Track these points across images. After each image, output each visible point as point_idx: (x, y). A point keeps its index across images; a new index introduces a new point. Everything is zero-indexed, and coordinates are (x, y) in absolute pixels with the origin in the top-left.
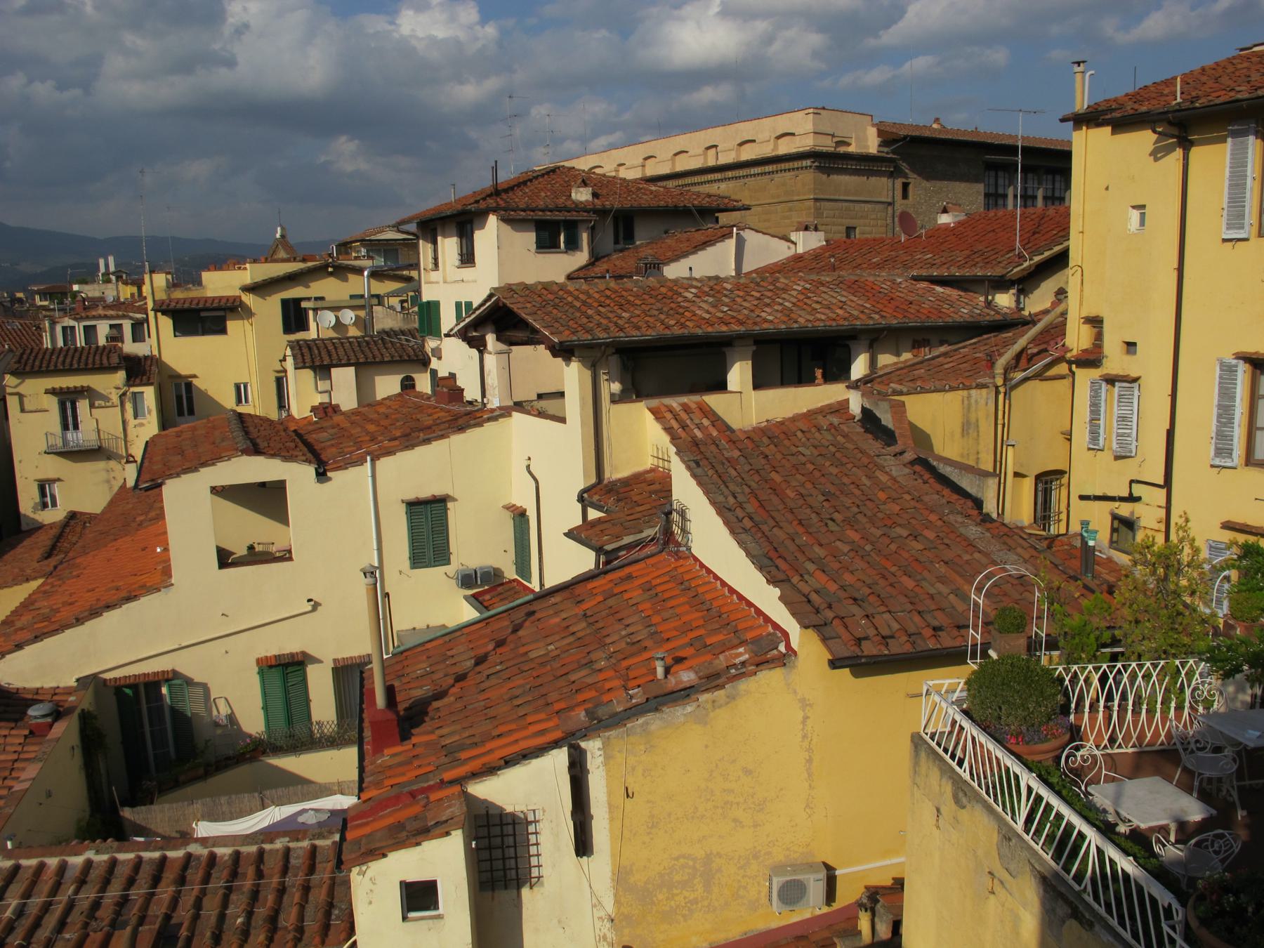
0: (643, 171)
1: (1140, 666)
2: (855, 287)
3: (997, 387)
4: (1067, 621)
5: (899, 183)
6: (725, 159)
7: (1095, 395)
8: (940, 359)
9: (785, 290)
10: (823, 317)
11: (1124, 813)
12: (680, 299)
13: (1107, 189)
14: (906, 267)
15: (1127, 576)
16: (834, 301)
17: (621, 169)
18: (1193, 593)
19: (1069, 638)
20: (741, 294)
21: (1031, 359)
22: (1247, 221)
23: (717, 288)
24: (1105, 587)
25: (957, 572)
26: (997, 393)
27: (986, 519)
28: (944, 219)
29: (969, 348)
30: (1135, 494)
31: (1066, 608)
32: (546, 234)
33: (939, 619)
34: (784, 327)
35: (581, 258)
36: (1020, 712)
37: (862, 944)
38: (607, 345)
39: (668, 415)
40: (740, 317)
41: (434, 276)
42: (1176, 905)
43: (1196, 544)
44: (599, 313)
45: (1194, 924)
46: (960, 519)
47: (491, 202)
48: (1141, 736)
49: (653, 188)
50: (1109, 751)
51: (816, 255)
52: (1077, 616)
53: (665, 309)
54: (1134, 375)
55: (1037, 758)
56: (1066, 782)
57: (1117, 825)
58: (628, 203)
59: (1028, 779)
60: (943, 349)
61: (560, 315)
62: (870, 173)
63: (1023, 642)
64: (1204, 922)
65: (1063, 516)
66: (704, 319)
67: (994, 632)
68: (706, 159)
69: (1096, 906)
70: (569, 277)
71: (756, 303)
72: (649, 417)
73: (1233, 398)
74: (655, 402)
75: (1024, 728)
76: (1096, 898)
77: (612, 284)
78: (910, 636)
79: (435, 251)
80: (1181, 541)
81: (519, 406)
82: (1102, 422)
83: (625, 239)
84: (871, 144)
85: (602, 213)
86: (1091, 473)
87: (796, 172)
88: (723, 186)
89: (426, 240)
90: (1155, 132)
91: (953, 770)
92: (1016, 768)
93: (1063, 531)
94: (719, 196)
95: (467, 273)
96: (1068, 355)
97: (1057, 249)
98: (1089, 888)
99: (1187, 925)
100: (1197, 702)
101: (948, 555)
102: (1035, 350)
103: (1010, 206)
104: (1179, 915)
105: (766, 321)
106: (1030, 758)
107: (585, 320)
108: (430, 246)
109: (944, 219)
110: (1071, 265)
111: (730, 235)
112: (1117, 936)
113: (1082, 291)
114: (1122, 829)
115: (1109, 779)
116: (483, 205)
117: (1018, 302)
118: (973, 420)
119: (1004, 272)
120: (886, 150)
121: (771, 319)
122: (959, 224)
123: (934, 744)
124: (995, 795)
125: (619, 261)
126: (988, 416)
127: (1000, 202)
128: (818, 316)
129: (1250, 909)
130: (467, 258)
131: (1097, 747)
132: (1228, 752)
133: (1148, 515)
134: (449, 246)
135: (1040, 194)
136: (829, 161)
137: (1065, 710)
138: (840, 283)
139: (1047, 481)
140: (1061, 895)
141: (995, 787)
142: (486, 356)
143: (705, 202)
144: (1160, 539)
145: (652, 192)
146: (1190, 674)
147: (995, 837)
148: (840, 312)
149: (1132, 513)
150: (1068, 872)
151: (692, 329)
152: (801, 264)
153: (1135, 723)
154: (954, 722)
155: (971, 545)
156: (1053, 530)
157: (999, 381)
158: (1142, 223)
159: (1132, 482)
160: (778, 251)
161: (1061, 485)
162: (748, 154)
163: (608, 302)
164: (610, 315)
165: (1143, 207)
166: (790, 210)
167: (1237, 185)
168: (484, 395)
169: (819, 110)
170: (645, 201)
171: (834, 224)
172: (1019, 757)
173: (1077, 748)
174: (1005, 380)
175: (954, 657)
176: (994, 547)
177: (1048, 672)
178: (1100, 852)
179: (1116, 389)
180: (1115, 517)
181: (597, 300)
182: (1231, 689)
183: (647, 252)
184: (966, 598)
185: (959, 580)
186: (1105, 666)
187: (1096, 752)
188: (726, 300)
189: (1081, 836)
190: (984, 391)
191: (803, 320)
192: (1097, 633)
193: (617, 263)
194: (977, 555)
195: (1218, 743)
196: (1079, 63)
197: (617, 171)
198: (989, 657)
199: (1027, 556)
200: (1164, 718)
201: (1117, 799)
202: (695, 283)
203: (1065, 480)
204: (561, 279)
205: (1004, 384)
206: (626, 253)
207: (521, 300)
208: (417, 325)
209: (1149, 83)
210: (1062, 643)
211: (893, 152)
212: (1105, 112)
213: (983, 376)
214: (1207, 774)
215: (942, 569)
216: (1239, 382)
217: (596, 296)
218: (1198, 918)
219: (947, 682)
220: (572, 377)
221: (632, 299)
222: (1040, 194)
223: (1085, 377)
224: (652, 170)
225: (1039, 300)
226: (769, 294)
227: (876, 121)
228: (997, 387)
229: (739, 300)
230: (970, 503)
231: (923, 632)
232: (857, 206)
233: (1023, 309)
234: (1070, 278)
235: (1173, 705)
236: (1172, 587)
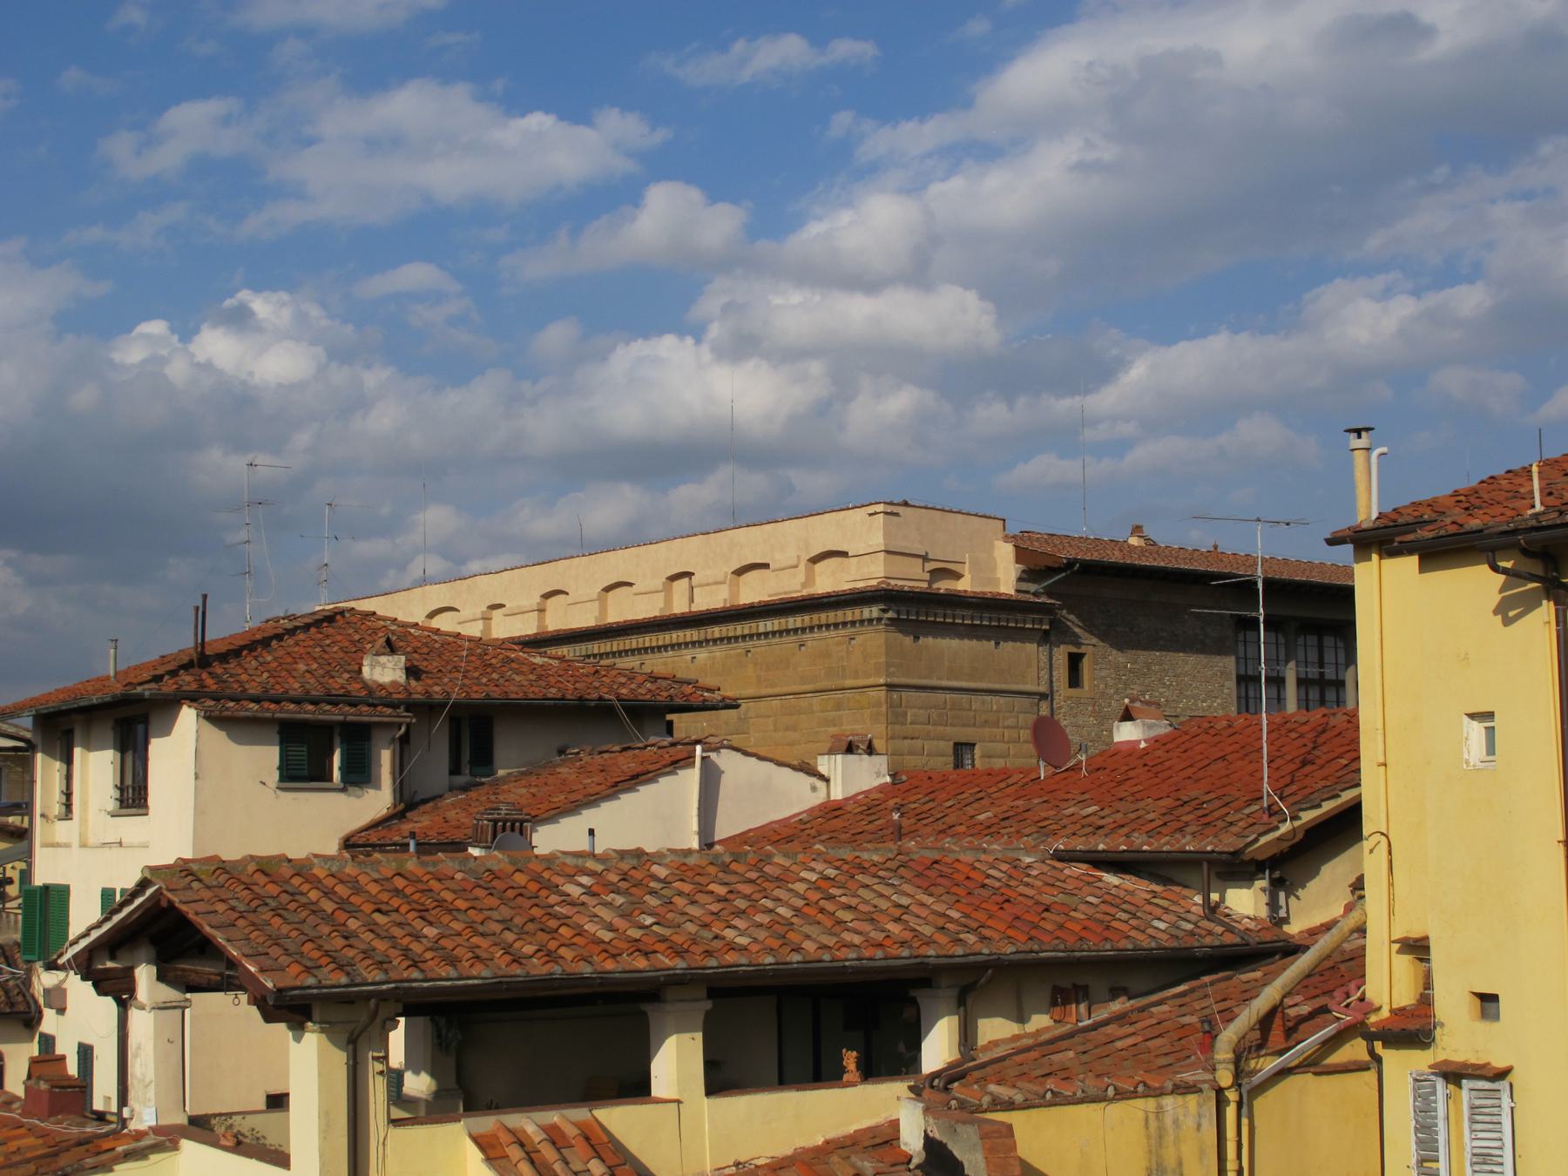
0: (541, 620)
2: (931, 875)
3: (1220, 1091)
5: (1061, 654)
6: (709, 600)
7: (1424, 1110)
8: (1109, 1029)
9: (781, 881)
10: (857, 940)
12: (554, 899)
14: (1045, 832)
16: (884, 904)
17: (497, 614)
20: (687, 888)
21: (1293, 1030)
23: (638, 875)
28: (1127, 733)
29: (1169, 1005)
32: (301, 751)
34: (769, 959)
35: (377, 801)
38: (382, 997)
39: (515, 1153)
40: (679, 939)
41: (62, 831)
44: (372, 928)
47: (187, 680)
49: (538, 660)
51: (869, 805)
53: (518, 920)
54: (1499, 1063)
58: (481, 689)
60: (1117, 1006)
61: (285, 929)
62: (1002, 634)
66: (600, 943)
68: (668, 600)
70: (348, 843)
71: (715, 907)
72: (474, 1154)
74: (487, 1123)
77: (411, 864)
79: (69, 778)
81: (201, 1127)
83: (472, 763)
84: (1004, 577)
85: (426, 709)
87: (849, 630)
88: (702, 655)
89: (49, 752)
90: (1495, 569)
94: (674, 679)
95: (131, 827)
102: (1305, 1009)
105: (732, 947)
107: (340, 942)
108: (58, 765)
109: (1127, 733)
110: (1365, 832)
111: (688, 761)
113: (1391, 884)
116: (168, 686)
117: (1273, 905)
118: (1170, 1162)
120: (1033, 587)
121: (745, 944)
122: (1156, 741)
125: (455, 812)
126: (1202, 1153)
128: (847, 936)
130: (133, 796)
134: (97, 768)
136: (917, 609)
138: (902, 865)
142: (135, 1015)
143: (644, 692)
145: (534, 668)
148: (891, 927)
151: (572, 963)
152: (838, 823)
157: (1225, 1078)
158: (1491, 748)
160: (793, 796)
162: (753, 591)
163: (395, 902)
164: (397, 932)
165: (1489, 715)
166: (839, 706)
168: (123, 1099)
169: (896, 507)
170: (518, 686)
171: (928, 737)
174: (1239, 1074)
179: (1465, 1094)
181: (372, 899)
183: (516, 795)
188: (652, 901)
190: (1192, 1099)
191: (814, 946)
193: (451, 815)
196: (1358, 432)
197: (486, 619)
202: (591, 864)
204: (332, 848)
205: (1237, 1084)
206: (473, 794)
207: (206, 894)
208: (18, 936)
209: (1499, 471)
211: (1049, 592)
212: (1410, 527)
217: (373, 889)
220: (306, 1062)
221: (448, 896)
223: (1401, 1065)
224: (560, 619)
225: (1315, 905)
226: (747, 889)
227: (1014, 529)
228: (1220, 1091)
229: (680, 902)
232: (977, 700)
233: (1286, 920)
234: (1369, 858)
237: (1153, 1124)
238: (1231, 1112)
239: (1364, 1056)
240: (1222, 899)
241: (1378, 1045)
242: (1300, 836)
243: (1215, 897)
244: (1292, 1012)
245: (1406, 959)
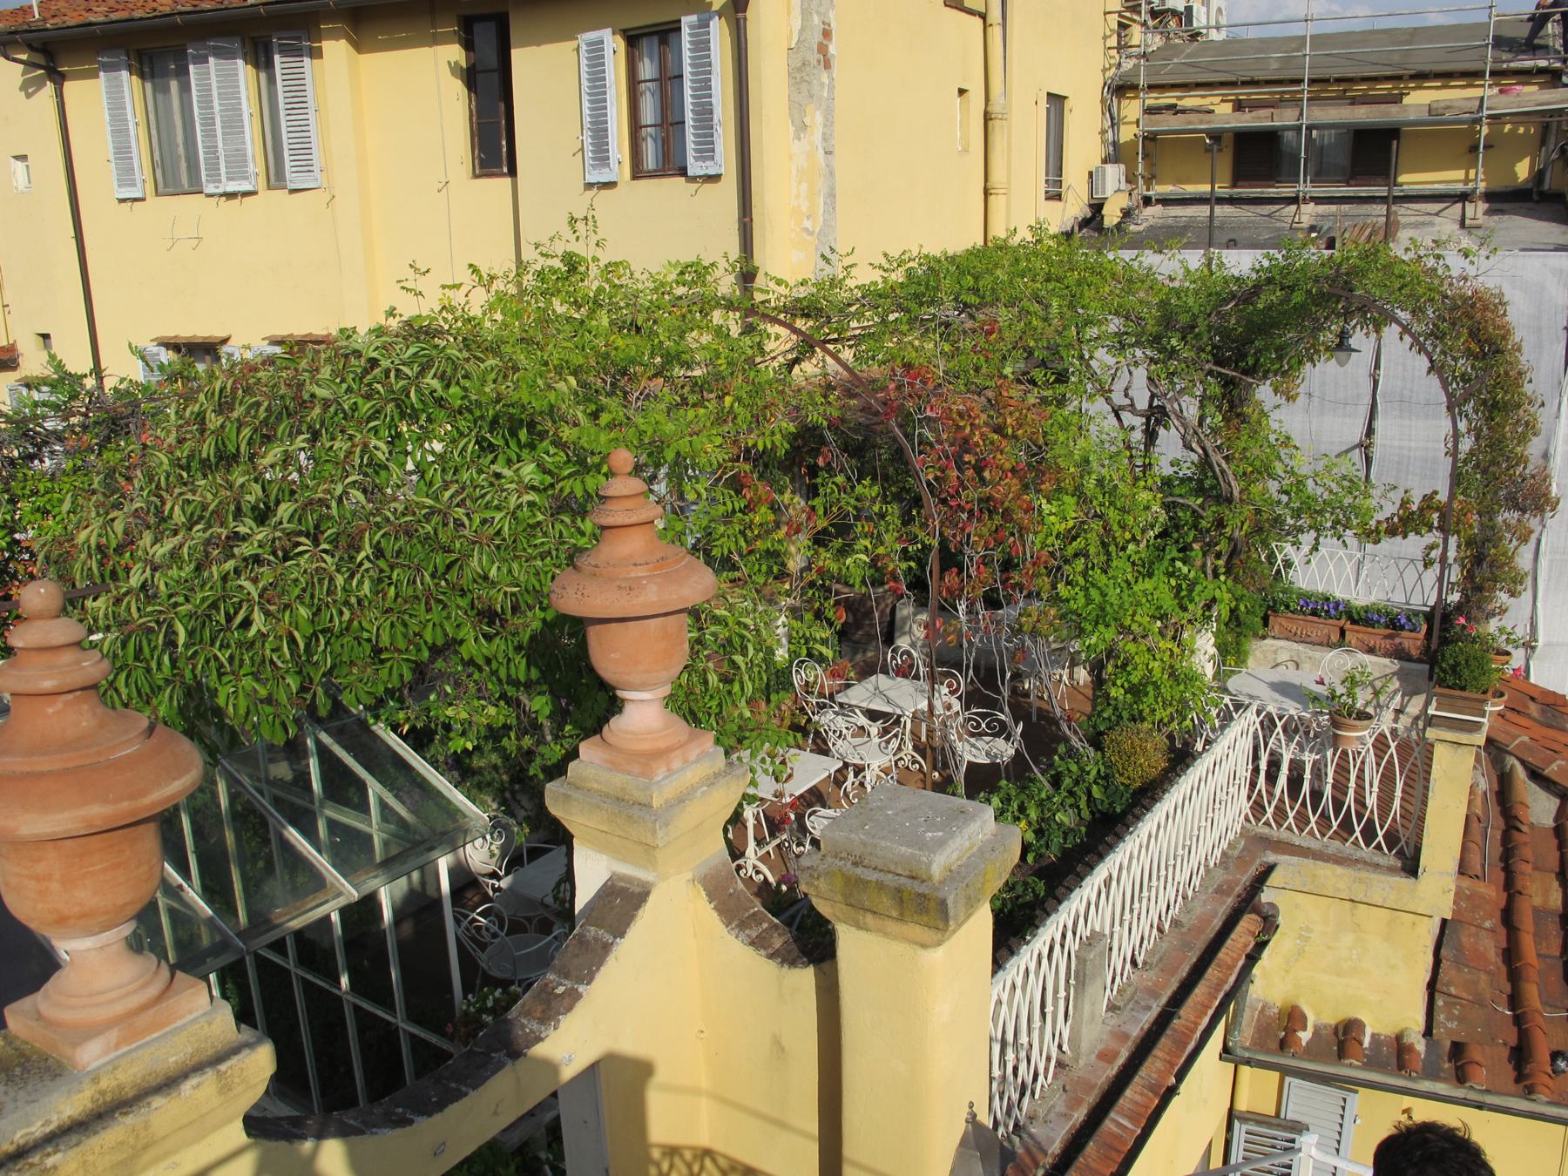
22: (251, 168)
167: (120, 131)
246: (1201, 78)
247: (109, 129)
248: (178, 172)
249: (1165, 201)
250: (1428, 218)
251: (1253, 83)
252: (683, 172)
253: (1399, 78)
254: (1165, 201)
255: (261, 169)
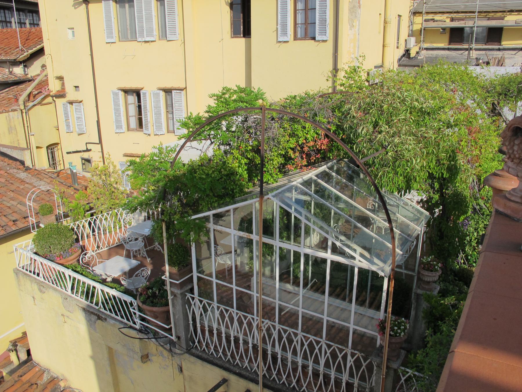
1: (103, 215)
4: (70, 204)
11: (108, 274)
13: (56, 20)
15: (90, 181)
18: (117, 183)
19: (72, 211)
24: (84, 188)
25: (19, 194)
26: (22, 113)
27: (27, 169)
30: (89, 149)
31: (69, 199)
33: (15, 217)
36: (58, 246)
37: (15, 366)
42: (133, 300)
43: (114, 164)
45: (140, 304)
46: (15, 171)
48: (109, 243)
50: (98, 251)
52: (74, 201)
54: (81, 100)
55: (70, 263)
56: (83, 268)
57: (106, 279)
59: (68, 272)
63: (54, 217)
64: (144, 303)
65: (62, 162)
67: (40, 216)
69: (106, 312)
73: (119, 105)
75: (62, 253)
76: (105, 309)
78: (2, 227)
80: (109, 164)
82: (70, 121)
86: (69, 142)
91: (36, 279)
92: (62, 269)
93: (63, 168)
96: (51, 94)
97: (39, 47)
98: (102, 306)
99: (139, 306)
100: (126, 224)
101: (13, 188)
102: (36, 92)
103: (14, 27)
104: (135, 304)
106: (67, 264)
112: (116, 320)
114: (109, 279)
115: (100, 262)
117: (25, 71)
119: (16, 58)
123: (24, 271)
124: (57, 283)
127: (9, 25)
129: (157, 292)
131: (93, 251)
132: (140, 239)
133: (95, 155)
135: (27, 22)
137: (77, 240)
139: (51, 148)
140: (92, 313)
141: (55, 280)
144: (101, 165)
146: (121, 214)
147: (61, 300)
149: (89, 156)
150: (92, 303)
153: (105, 238)
154: (31, 259)
155: (23, 181)
156: (59, 169)
157: (22, 107)
158: (74, 36)
159: (86, 143)
161: (58, 149)
165: (73, 28)
172: (62, 265)
173: (85, 254)
175: (26, 231)
176: (34, 180)
177: (66, 227)
178: (102, 291)
180: (83, 159)
182: (137, 216)
184: (25, 205)
185: (20, 197)
186: (89, 219)
187: (93, 253)
189: (94, 287)
190: (16, 112)
192: (83, 207)
194: (26, 185)
195: (136, 237)
198: (41, 227)
199: (49, 181)
200: (116, 233)
201: (104, 269)
203: (59, 147)
210: (70, 214)
213: (14, 106)
214: (135, 249)
215: (12, 194)
216: (120, 99)
218: (142, 302)
219: (24, 242)
222: (27, 22)
225: (34, 70)
230: (18, 163)
231: (9, 224)
233: (27, 74)
235: (118, 227)
236: (109, 182)
237: (8, 118)
238: (24, 114)
239: (52, 101)
240: (13, 70)
241: (54, 98)
242: (29, 56)
243: (11, 70)
244: (34, 93)
245: (58, 81)
246: (441, 10)
247: (105, 20)
248: (129, 33)
249: (427, 49)
250: (512, 56)
251: (458, 12)
252: (314, 38)
253: (504, 12)
254: (427, 49)
255: (157, 34)
